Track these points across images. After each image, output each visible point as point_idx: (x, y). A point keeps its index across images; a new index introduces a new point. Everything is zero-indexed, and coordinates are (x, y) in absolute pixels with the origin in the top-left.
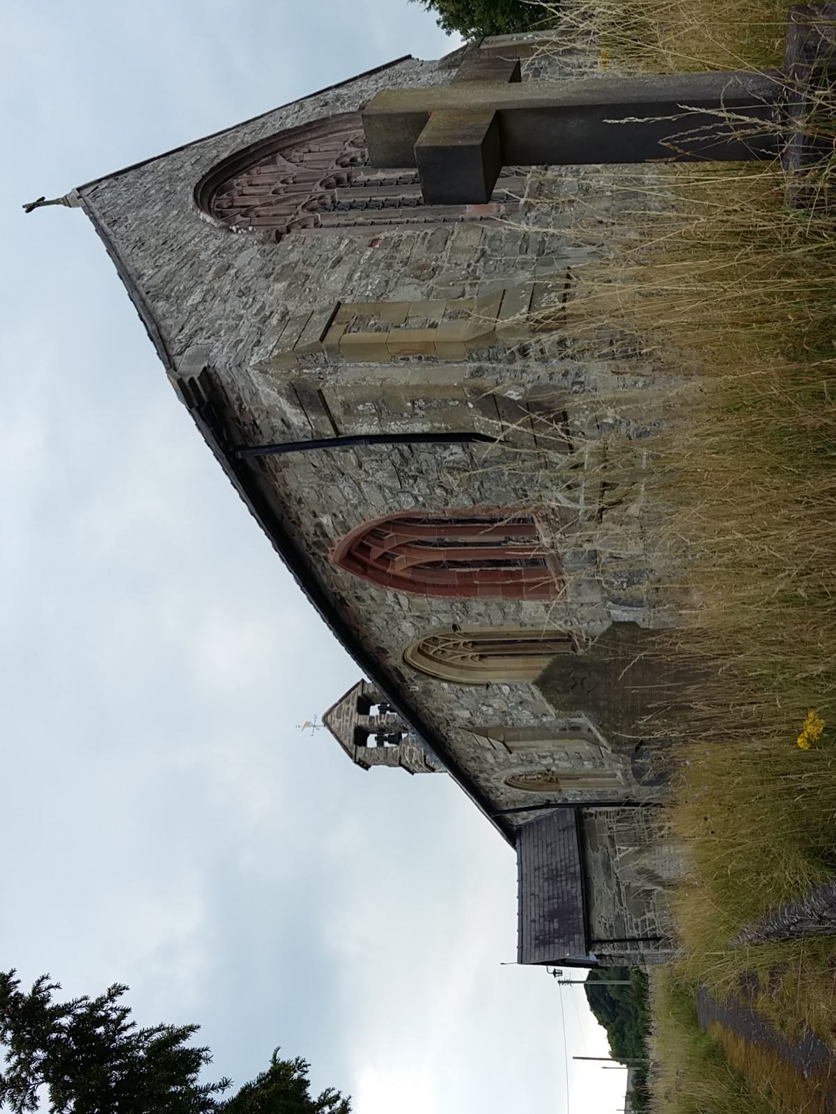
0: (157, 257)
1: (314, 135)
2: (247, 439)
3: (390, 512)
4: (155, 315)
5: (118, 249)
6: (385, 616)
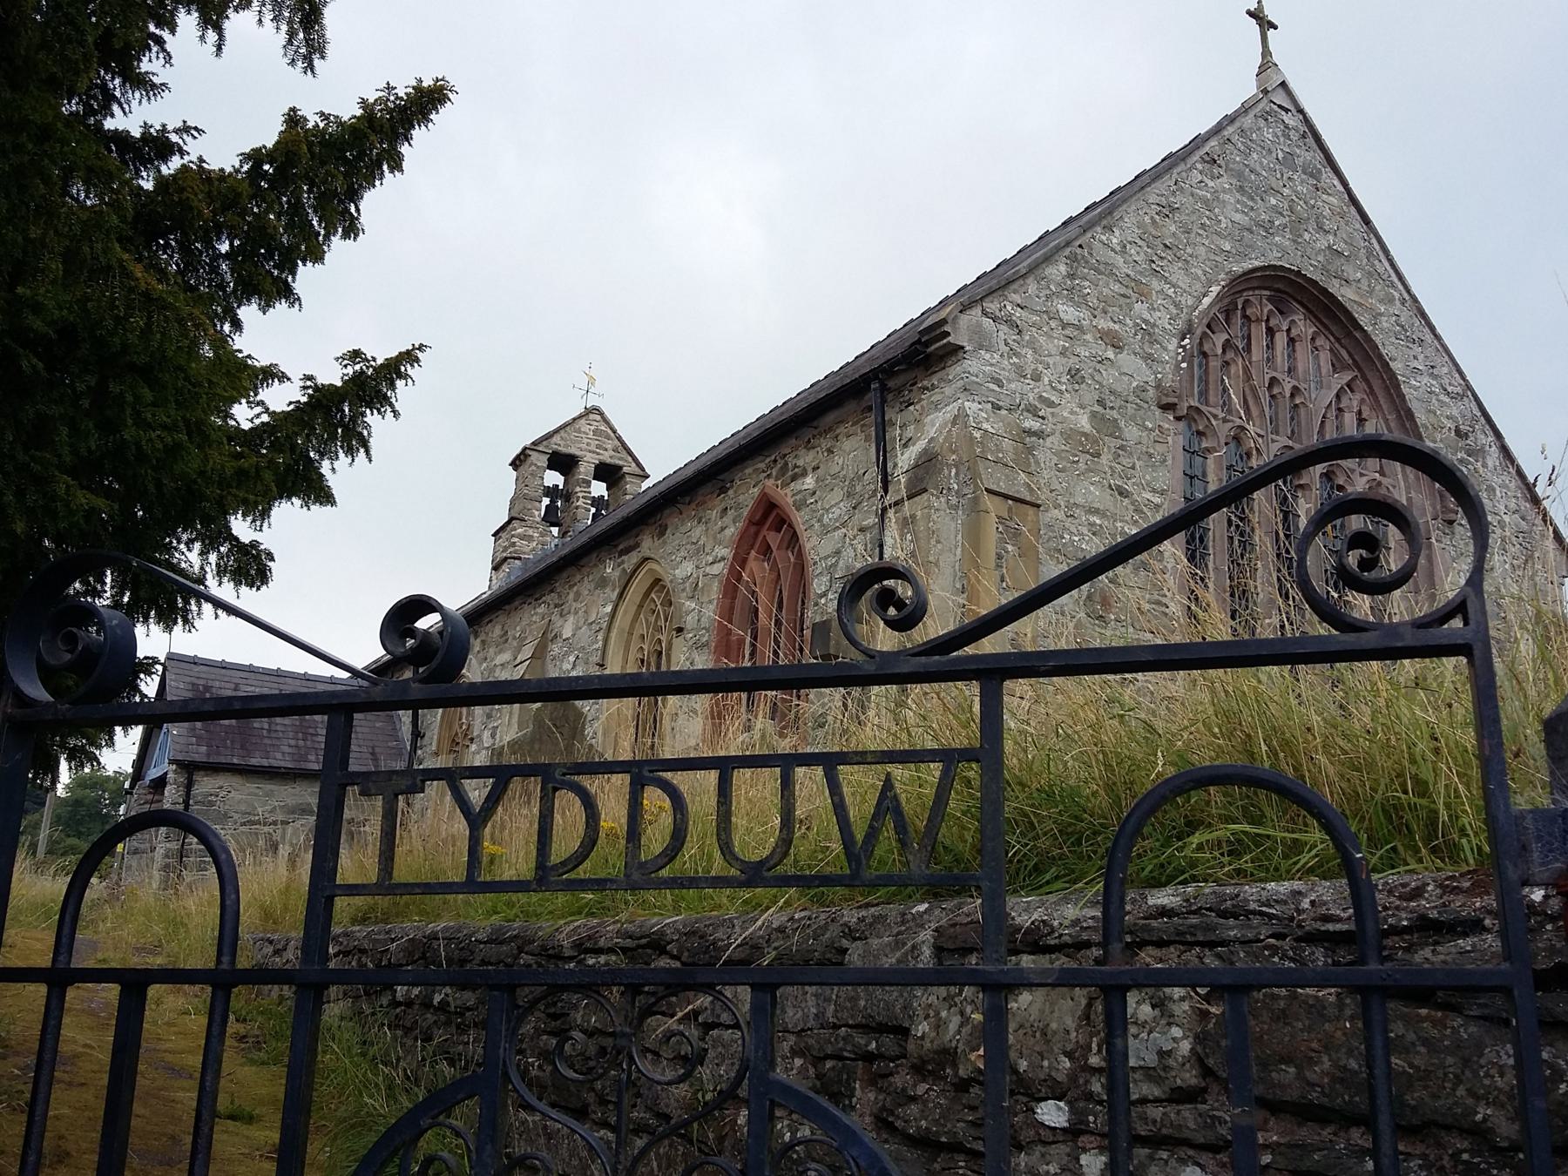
0: (1140, 242)
1: (1392, 425)
2: (896, 393)
3: (812, 562)
4: (1044, 265)
5: (1157, 184)
6: (701, 542)
